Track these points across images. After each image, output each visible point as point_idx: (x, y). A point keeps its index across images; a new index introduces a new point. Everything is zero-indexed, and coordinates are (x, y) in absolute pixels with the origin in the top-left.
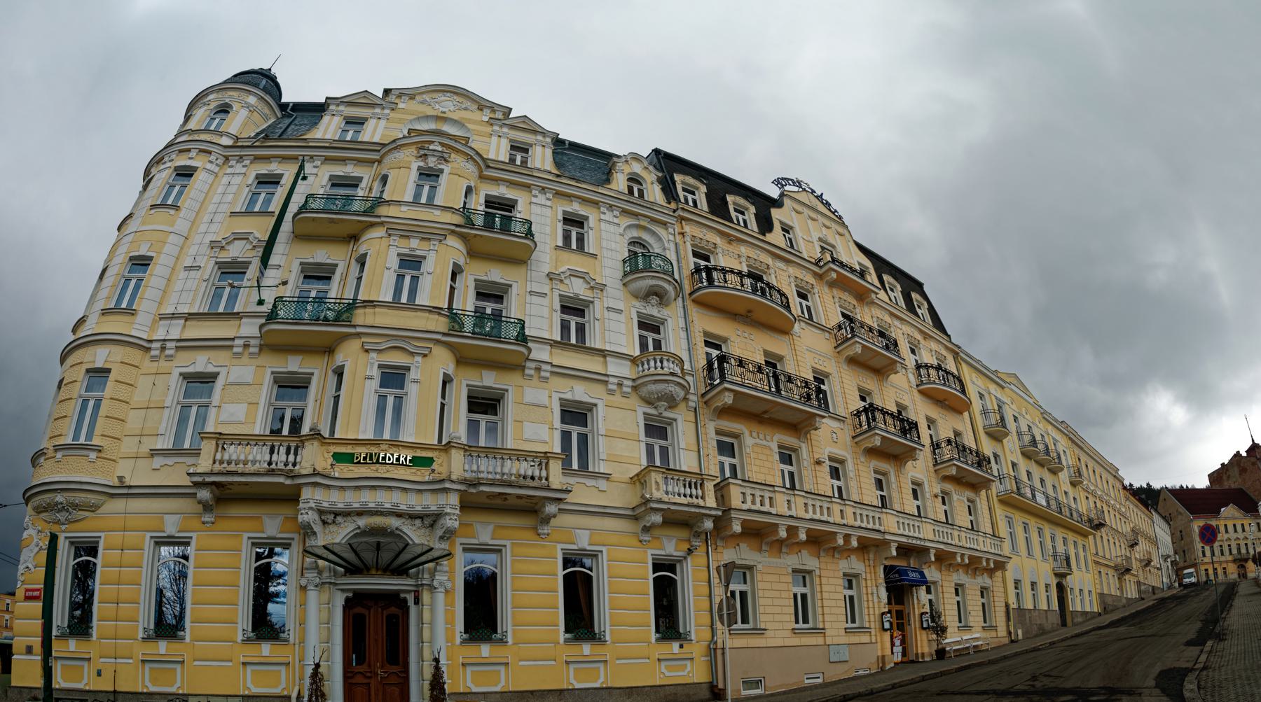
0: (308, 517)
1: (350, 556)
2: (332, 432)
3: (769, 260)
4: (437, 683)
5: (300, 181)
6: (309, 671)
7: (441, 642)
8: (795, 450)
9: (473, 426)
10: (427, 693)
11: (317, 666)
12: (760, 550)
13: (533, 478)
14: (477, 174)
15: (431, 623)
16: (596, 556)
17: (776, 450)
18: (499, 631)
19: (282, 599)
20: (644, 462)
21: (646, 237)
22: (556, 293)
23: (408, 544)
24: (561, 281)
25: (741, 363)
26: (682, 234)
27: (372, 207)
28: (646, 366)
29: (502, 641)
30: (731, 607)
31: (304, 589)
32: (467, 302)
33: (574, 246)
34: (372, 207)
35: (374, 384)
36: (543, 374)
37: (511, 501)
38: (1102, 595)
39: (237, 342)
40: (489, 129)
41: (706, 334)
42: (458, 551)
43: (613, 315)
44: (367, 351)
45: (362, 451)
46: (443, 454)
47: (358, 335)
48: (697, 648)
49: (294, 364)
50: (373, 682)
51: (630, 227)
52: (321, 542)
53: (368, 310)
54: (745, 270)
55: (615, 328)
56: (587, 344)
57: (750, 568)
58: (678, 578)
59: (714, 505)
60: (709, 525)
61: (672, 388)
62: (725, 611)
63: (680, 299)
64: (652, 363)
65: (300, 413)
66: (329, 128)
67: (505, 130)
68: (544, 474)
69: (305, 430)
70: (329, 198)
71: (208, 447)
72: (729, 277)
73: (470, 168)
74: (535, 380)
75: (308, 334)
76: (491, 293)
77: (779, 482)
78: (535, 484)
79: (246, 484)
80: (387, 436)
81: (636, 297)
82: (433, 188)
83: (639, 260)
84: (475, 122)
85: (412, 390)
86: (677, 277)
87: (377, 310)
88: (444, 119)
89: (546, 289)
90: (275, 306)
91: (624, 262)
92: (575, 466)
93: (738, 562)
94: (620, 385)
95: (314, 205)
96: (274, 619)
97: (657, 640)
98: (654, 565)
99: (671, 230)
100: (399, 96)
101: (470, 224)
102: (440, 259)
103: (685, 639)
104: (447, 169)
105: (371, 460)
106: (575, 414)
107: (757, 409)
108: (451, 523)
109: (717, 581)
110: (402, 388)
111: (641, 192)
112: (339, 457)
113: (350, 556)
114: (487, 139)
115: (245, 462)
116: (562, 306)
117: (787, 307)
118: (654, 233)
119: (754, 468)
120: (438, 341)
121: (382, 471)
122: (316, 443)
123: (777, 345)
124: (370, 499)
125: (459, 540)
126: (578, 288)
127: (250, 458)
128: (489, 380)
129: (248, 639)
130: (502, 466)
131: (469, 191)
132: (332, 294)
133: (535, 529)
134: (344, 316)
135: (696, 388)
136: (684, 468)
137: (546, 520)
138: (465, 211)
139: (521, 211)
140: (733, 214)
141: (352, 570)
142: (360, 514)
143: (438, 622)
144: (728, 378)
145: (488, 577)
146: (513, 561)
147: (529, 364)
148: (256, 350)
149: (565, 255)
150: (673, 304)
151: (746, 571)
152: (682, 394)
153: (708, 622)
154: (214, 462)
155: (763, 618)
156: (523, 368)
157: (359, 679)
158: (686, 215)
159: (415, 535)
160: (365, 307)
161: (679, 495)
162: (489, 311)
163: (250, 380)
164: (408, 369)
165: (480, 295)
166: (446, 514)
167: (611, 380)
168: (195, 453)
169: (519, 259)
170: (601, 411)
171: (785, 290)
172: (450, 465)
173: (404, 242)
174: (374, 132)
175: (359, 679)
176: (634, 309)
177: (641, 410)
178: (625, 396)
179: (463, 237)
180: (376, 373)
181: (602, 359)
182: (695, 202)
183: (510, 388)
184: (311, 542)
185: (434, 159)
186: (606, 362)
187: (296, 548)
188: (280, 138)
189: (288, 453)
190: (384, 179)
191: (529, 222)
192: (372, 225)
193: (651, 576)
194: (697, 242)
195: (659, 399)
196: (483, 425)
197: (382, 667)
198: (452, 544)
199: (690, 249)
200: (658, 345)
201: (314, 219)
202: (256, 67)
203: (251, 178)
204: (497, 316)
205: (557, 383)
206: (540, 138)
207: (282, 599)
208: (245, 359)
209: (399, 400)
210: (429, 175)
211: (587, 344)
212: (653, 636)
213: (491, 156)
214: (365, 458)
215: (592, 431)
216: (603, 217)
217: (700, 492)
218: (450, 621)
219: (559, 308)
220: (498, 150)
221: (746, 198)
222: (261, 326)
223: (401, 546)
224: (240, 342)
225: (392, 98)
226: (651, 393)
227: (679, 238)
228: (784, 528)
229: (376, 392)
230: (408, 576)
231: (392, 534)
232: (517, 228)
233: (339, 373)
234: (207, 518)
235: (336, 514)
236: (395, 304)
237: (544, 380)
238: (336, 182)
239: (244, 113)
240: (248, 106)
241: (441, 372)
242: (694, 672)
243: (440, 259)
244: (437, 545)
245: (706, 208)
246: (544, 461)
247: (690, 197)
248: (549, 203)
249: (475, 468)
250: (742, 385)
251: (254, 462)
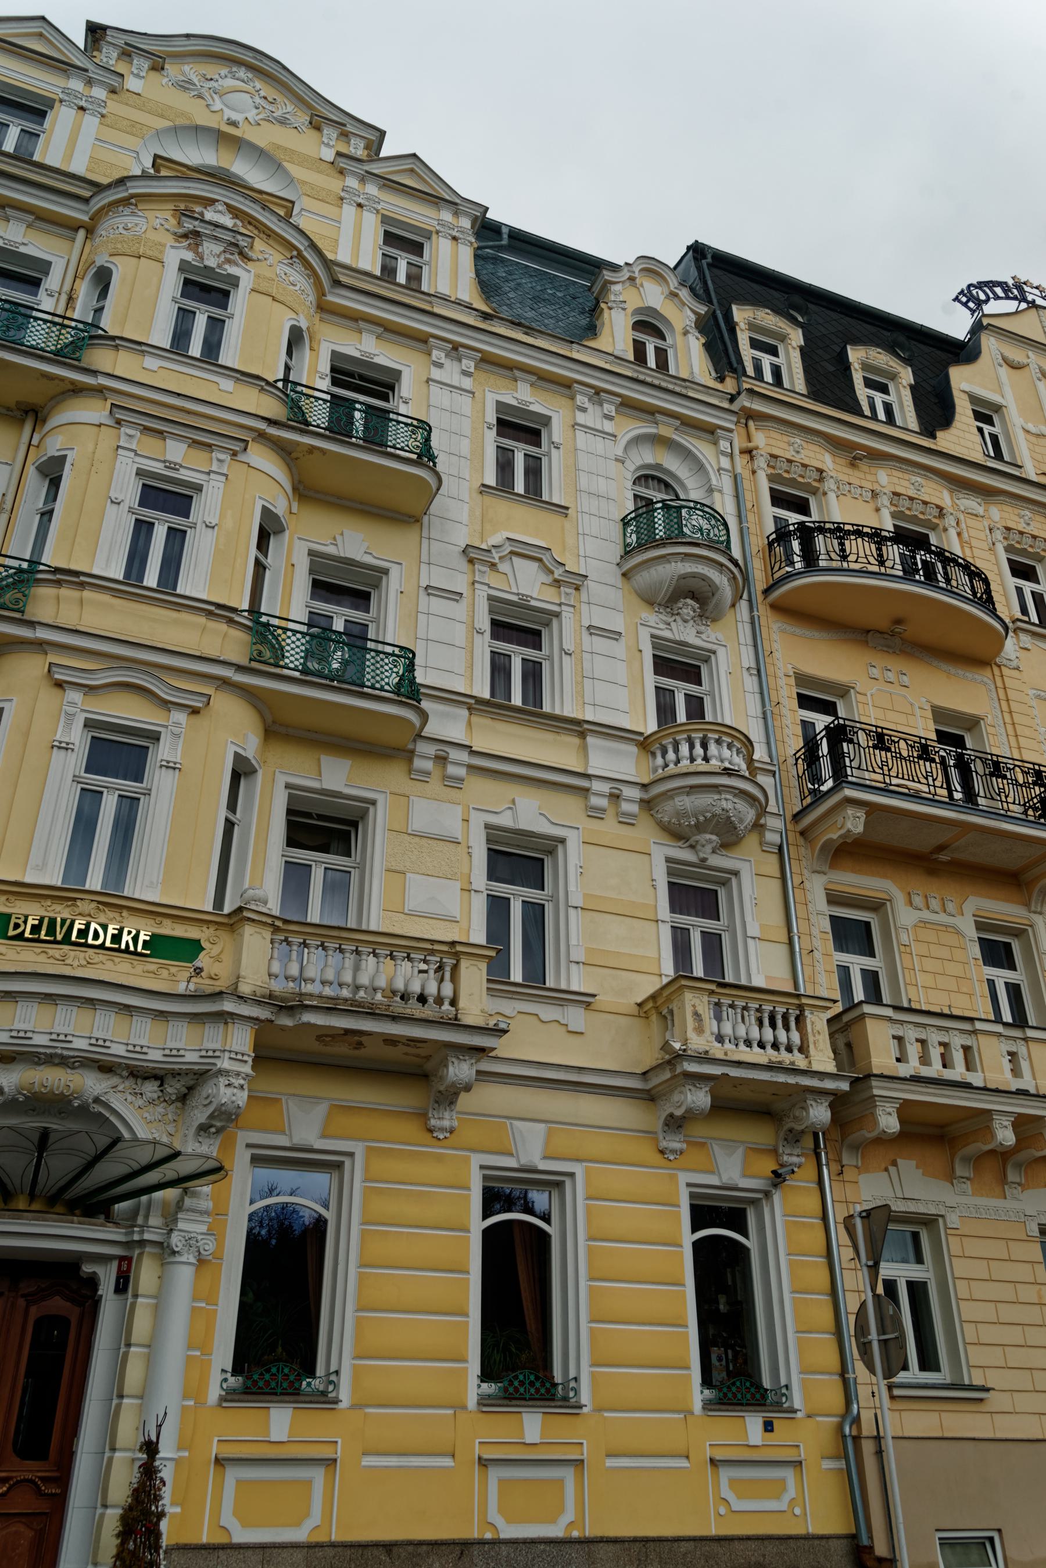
3: (943, 496)
4: (141, 1517)
7: (169, 1397)
8: (1019, 933)
9: (296, 878)
10: (109, 1544)
12: (951, 1177)
13: (422, 999)
14: (312, 298)
15: (151, 1346)
16: (559, 1185)
17: (974, 934)
18: (320, 1371)
20: (668, 969)
21: (672, 463)
22: (482, 593)
23: (117, 1140)
25: (881, 741)
26: (749, 452)
28: (671, 755)
29: (325, 1399)
30: (888, 1322)
32: (291, 601)
33: (520, 487)
35: (76, 761)
36: (451, 770)
37: (372, 1050)
40: (334, 184)
41: (801, 679)
42: (240, 1163)
43: (600, 644)
44: (59, 685)
45: (32, 912)
46: (224, 936)
47: (41, 646)
48: (808, 1435)
53: (65, 592)
54: (888, 525)
55: (605, 675)
56: (547, 708)
57: (930, 1222)
58: (751, 1243)
59: (831, 1067)
60: (820, 1113)
61: (727, 803)
62: (874, 1336)
63: (744, 605)
64: (684, 749)
67: (372, 189)
68: (447, 990)
72: (852, 545)
73: (297, 280)
76: (344, 586)
77: (984, 1009)
78: (428, 1012)
81: (650, 603)
83: (656, 517)
84: (304, 161)
85: (161, 787)
86: (736, 552)
87: (87, 594)
88: (236, 143)
89: (460, 584)
91: (625, 522)
92: (517, 974)
93: (898, 1206)
97: (707, 1405)
98: (695, 1209)
99: (724, 445)
100: (126, 54)
101: (299, 421)
102: (237, 492)
103: (778, 1406)
104: (246, 276)
105: (50, 933)
106: (519, 859)
107: (923, 841)
108: (229, 1093)
109: (848, 1253)
110: (138, 777)
111: (661, 354)
114: (329, 210)
116: (494, 623)
117: (987, 602)
118: (687, 454)
119: (921, 979)
120: (225, 683)
121: (75, 962)
123: (963, 693)
125: (244, 1137)
126: (527, 583)
128: (336, 777)
130: (357, 968)
131: (296, 339)
133: (423, 1116)
135: (782, 801)
136: (758, 981)
137: (449, 1097)
138: (288, 389)
139: (410, 399)
140: (862, 393)
144: (853, 775)
145: (306, 1230)
146: (367, 1192)
147: (422, 748)
150: (729, 618)
151: (917, 1233)
152: (750, 815)
153: (832, 1360)
155: (976, 1356)
156: (409, 755)
158: (758, 406)
160: (59, 583)
161: (748, 1043)
162: (339, 625)
164: (155, 737)
165: (321, 588)
166: (221, 1072)
167: (597, 786)
169: (403, 510)
170: (574, 854)
171: (982, 562)
172: (238, 962)
173: (150, 445)
176: (643, 629)
177: (661, 852)
178: (627, 821)
179: (284, 451)
180: (78, 737)
181: (576, 741)
182: (776, 371)
183: (380, 798)
185: (218, 248)
190: (103, 279)
192: (77, 390)
193: (688, 1238)
194: (781, 468)
195: (699, 828)
196: (317, 876)
198: (228, 1146)
199: (764, 486)
200: (696, 707)
204: (357, 638)
205: (480, 789)
206: (446, 216)
209: (129, 806)
211: (547, 708)
212: (697, 1396)
213: (343, 256)
214: (36, 929)
215: (554, 898)
217: (796, 1037)
218: (199, 1342)
220: (356, 241)
221: (891, 349)
223: (103, 1141)
225: (108, 55)
226: (682, 814)
227: (740, 461)
228: (1007, 1121)
229: (76, 779)
230: (109, 1217)
231: (84, 1112)
232: (400, 437)
237: (454, 783)
241: (231, 750)
242: (807, 1504)
243: (237, 492)
244: (190, 1146)
245: (801, 386)
246: (449, 961)
247: (767, 360)
248: (467, 383)
249: (294, 970)
250: (886, 791)
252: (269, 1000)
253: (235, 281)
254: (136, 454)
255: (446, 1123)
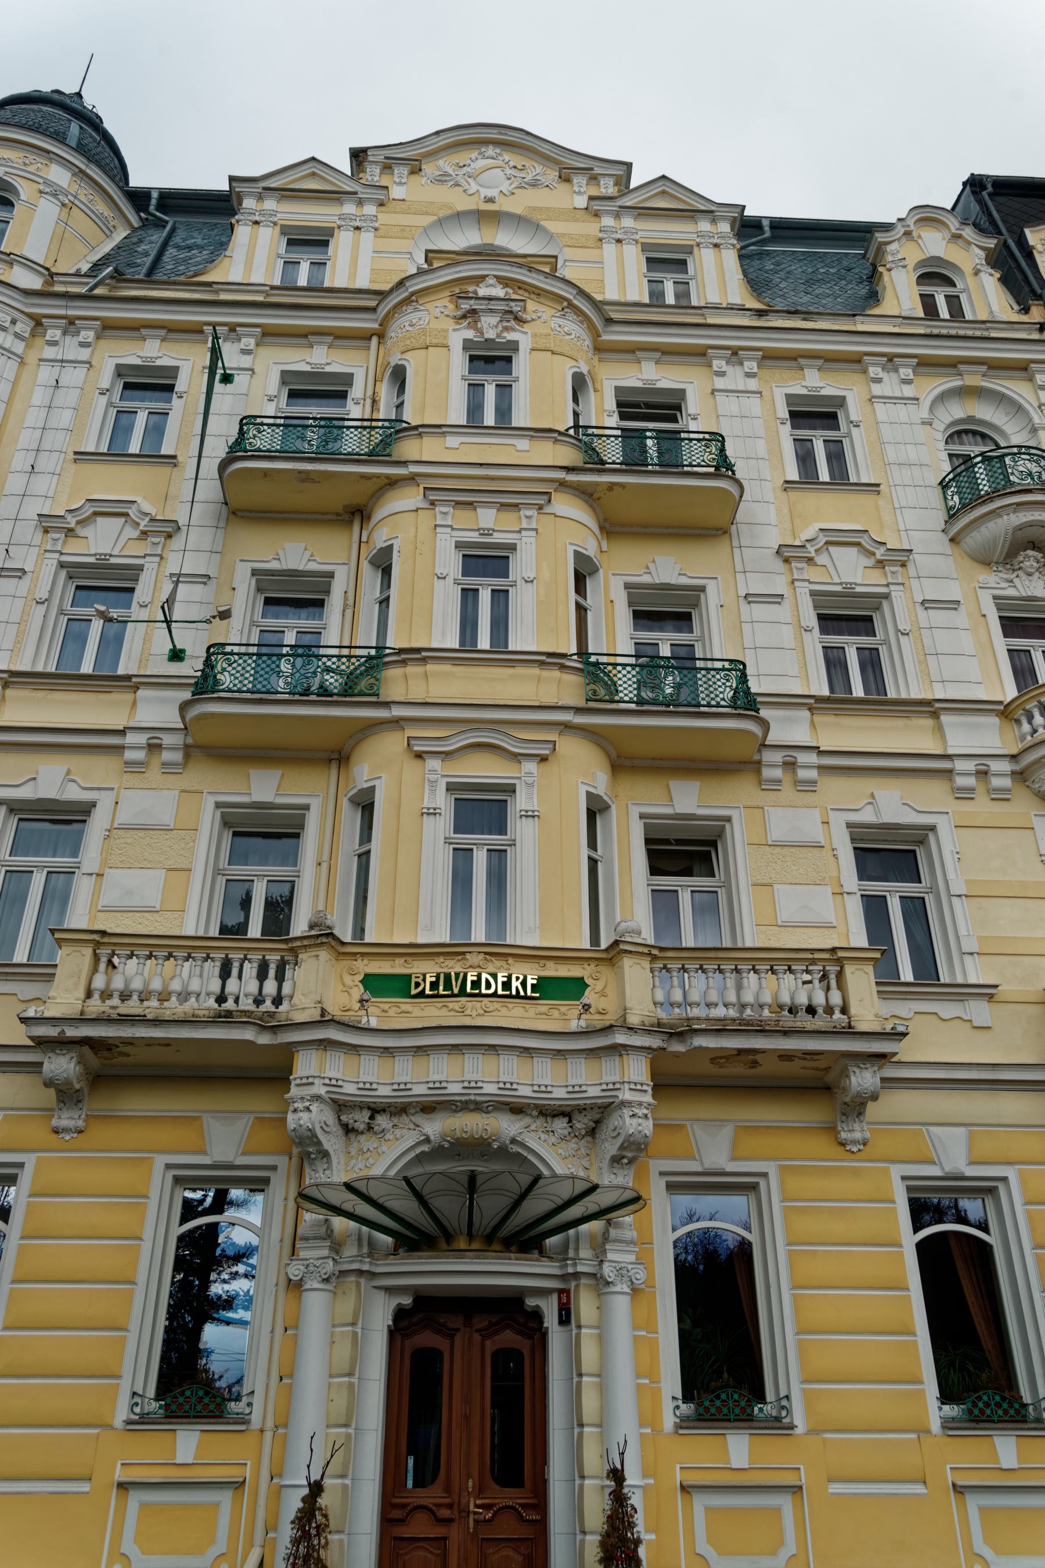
0: (312, 1118)
1: (406, 1206)
2: (360, 929)
5: (218, 387)
6: (293, 1503)
7: (626, 1425)
9: (664, 905)
11: (316, 1489)
13: (811, 1010)
15: (601, 1374)
16: (992, 1191)
18: (770, 1396)
19: (241, 1314)
21: (985, 412)
22: (803, 591)
23: (538, 1178)
24: (810, 560)
27: (386, 443)
29: (780, 1424)
31: (295, 1287)
32: (616, 636)
33: (824, 475)
34: (386, 443)
35: (443, 825)
36: (802, 774)
37: (769, 1067)
38: (212, 1352)
39: (131, 738)
40: (591, 228)
42: (656, 1192)
43: (937, 617)
44: (419, 756)
45: (428, 970)
46: (605, 971)
47: (398, 723)
49: (264, 787)
50: (454, 1534)
51: (943, 397)
52: (340, 1175)
53: (411, 670)
56: (892, 694)
65: (285, 890)
66: (252, 256)
67: (628, 222)
68: (836, 998)
69: (299, 926)
70: (291, 424)
71: (73, 963)
74: (787, 787)
75: (287, 719)
76: (663, 611)
78: (819, 1022)
79: (166, 1043)
80: (479, 934)
82: (504, 390)
85: (525, 836)
87: (430, 667)
89: (780, 585)
90: (208, 664)
91: (944, 485)
94: (983, 774)
95: (264, 440)
96: (215, 1365)
100: (387, 168)
101: (596, 462)
102: (548, 542)
104: (523, 338)
105: (448, 988)
106: (889, 856)
108: (635, 1123)
110: (502, 830)
112: (377, 985)
113: (406, 1206)
114: (591, 254)
115: (164, 997)
116: (821, 618)
118: (1000, 399)
120: (566, 727)
122: (324, 954)
124: (450, 1074)
125: (656, 1165)
126: (849, 570)
127: (176, 986)
128: (687, 800)
129: (144, 1419)
130: (739, 987)
131: (579, 385)
132: (332, 636)
133: (831, 1130)
134: (363, 684)
137: (857, 1107)
138: (580, 434)
139: (698, 415)
141: (413, 1240)
142: (428, 1108)
143: (616, 1370)
145: (731, 1254)
146: (787, 1211)
147: (768, 756)
148: (178, 756)
149: (809, 500)
154: (89, 994)
156: (757, 766)
157: (420, 1527)
159: (556, 1155)
160: (404, 662)
162: (665, 651)
163: (167, 818)
164: (511, 790)
165: (643, 617)
166: (624, 1104)
168: (42, 972)
170: (948, 841)
173: (464, 518)
174: (355, 262)
175: (420, 1527)
176: (983, 592)
178: (1000, 796)
179: (587, 494)
180: (443, 802)
181: (929, 722)
183: (734, 814)
184: (315, 1176)
185: (494, 320)
186: (940, 729)
187: (282, 1188)
188: (150, 277)
189: (262, 975)
190: (399, 376)
191: (718, 438)
192: (392, 483)
196: (685, 900)
197: (480, 1491)
198: (642, 1175)
201: (266, 473)
202: (46, 87)
203: (106, 377)
204: (685, 660)
206: (704, 226)
207: (241, 1314)
208: (154, 774)
209: (498, 858)
210: (490, 360)
211: (892, 694)
214: (434, 985)
215: (934, 889)
216: (877, 389)
218: (646, 1369)
219: (814, 623)
222: (184, 707)
223: (525, 1180)
224: (142, 739)
225: (373, 174)
229: (448, 841)
230: (542, 1252)
232: (695, 455)
233: (365, 805)
234: (66, 1119)
235: (375, 1111)
236: (466, 652)
238: (302, 388)
239: (48, 210)
240: (56, 192)
244: (606, 1178)
248: (753, 384)
251: (184, 996)
252: (657, 1028)
253: (514, 346)
254: (453, 529)
255: (857, 1135)
